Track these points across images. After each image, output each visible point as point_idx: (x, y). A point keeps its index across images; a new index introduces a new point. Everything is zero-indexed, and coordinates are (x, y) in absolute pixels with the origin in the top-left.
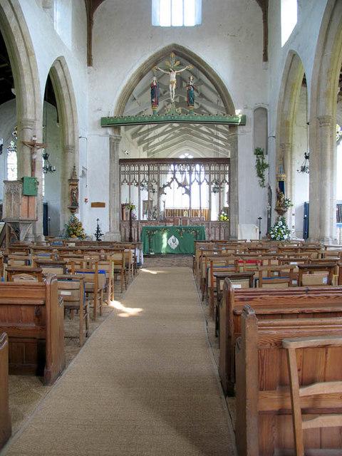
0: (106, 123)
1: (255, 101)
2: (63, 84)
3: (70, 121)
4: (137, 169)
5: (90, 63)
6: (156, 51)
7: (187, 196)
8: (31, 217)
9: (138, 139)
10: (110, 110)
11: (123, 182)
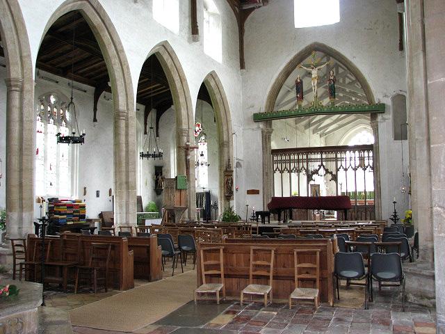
0: (258, 118)
1: (393, 90)
2: (216, 91)
3: (224, 121)
4: (296, 157)
5: (242, 66)
6: (300, 50)
7: (333, 182)
8: (183, 206)
9: (312, 128)
10: (261, 106)
11: (301, 169)
